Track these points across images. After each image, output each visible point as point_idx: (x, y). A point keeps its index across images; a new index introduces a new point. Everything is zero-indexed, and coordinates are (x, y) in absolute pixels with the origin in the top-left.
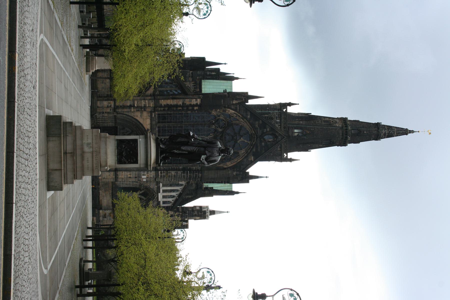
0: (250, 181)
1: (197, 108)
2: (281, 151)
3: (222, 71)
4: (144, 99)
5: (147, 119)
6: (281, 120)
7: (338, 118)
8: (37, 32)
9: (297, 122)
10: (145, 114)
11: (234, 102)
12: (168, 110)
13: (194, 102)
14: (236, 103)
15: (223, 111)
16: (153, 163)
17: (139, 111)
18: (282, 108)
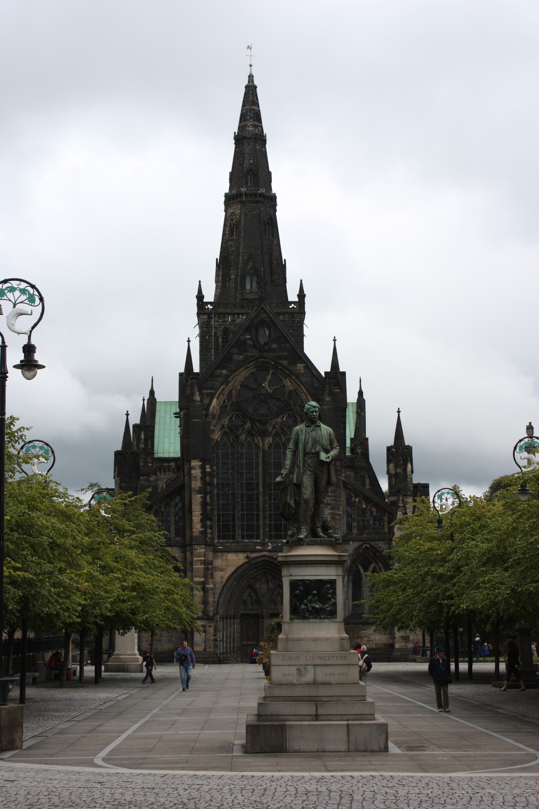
0: (342, 369)
1: (208, 466)
2: (284, 314)
4: (192, 564)
5: (227, 560)
6: (229, 314)
7: (226, 211)
8: (100, 774)
9: (232, 284)
10: (218, 562)
11: (197, 398)
12: (211, 520)
13: (197, 473)
14: (200, 395)
15: (213, 418)
16: (335, 550)
17: (212, 574)
18: (206, 311)
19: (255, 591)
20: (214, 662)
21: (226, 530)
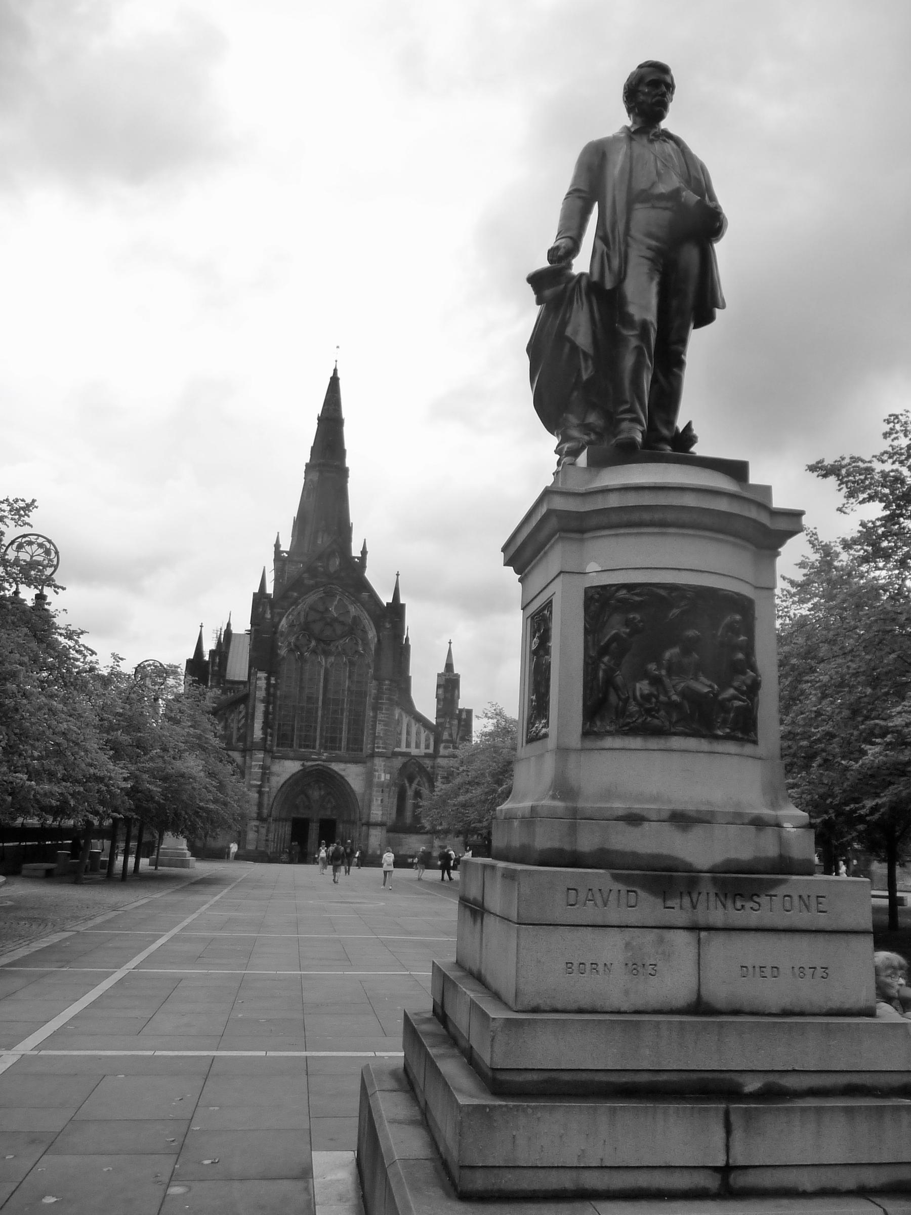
1: (273, 679)
3: (213, 647)
11: (268, 616)
12: (271, 728)
13: (262, 683)
15: (281, 636)
19: (307, 796)
20: (262, 861)
21: (281, 739)
